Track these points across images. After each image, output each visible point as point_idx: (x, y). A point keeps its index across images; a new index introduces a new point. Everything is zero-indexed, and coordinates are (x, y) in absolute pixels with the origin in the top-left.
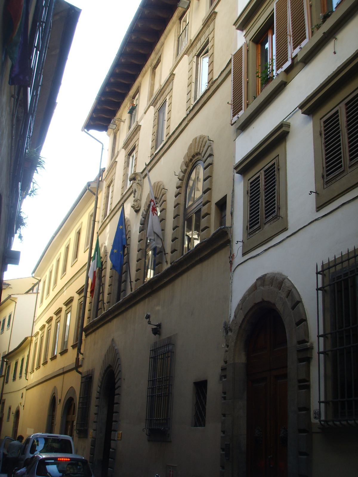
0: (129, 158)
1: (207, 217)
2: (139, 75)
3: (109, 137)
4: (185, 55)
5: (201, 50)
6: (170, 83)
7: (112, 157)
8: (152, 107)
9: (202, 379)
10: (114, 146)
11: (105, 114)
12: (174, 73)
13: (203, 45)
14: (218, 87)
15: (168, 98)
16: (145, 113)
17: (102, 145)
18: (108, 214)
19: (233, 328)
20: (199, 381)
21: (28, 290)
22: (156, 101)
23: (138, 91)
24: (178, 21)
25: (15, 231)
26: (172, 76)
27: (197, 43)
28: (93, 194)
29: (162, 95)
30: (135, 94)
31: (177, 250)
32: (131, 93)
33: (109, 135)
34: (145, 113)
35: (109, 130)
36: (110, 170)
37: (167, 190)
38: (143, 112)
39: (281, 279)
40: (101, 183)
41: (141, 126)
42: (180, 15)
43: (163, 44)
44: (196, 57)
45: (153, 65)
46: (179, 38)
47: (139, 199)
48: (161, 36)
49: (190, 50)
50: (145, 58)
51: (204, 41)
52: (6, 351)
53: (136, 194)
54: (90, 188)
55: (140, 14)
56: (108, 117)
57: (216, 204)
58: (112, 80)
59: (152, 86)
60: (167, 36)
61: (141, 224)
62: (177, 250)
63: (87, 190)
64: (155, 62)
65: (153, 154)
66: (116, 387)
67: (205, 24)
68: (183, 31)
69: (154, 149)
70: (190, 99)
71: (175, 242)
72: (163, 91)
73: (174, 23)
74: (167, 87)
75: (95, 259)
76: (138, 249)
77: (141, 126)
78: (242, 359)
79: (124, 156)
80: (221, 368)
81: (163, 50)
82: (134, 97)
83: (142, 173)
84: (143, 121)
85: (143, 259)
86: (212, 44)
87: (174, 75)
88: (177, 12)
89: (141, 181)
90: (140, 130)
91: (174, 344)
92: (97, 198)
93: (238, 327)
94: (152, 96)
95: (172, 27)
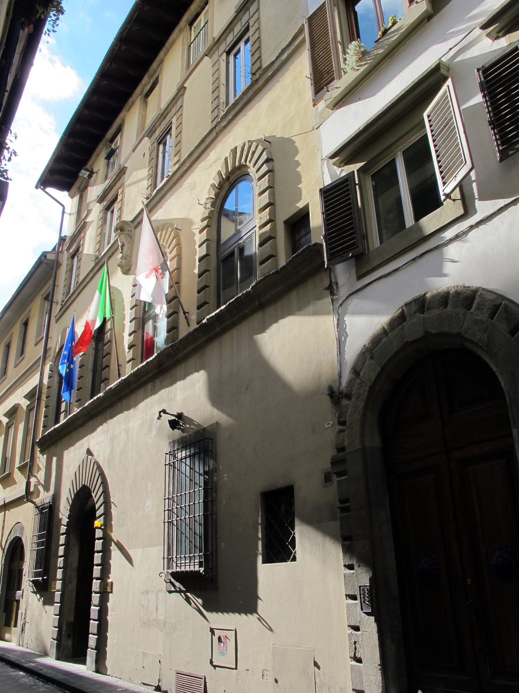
0: (106, 214)
4: (206, 57)
5: (242, 33)
6: (178, 100)
8: (146, 139)
9: (281, 484)
11: (67, 170)
12: (185, 85)
13: (237, 37)
15: (174, 120)
16: (134, 151)
17: (62, 208)
18: (71, 292)
19: (354, 392)
20: (273, 488)
21: (10, 297)
22: (154, 130)
23: (119, 130)
24: (188, 27)
25: (8, 88)
26: (182, 90)
27: (227, 36)
29: (163, 120)
30: (113, 135)
31: (208, 303)
32: (109, 134)
33: (72, 197)
34: (134, 151)
35: (74, 189)
37: (270, 142)
38: (131, 149)
39: (468, 292)
40: (60, 254)
41: (126, 168)
42: (190, 19)
43: (162, 61)
44: (225, 54)
45: (145, 92)
46: (190, 46)
47: (129, 255)
49: (214, 49)
50: (135, 82)
51: (241, 30)
53: (125, 248)
55: (135, 13)
56: (73, 169)
57: (286, 222)
58: (78, 127)
59: (143, 118)
60: (168, 50)
62: (208, 303)
64: (148, 87)
65: (64, 301)
66: (97, 516)
68: (195, 39)
69: (65, 296)
70: (179, 151)
71: (205, 291)
72: (165, 114)
73: (181, 31)
74: (173, 106)
77: (126, 168)
78: (374, 441)
79: (98, 211)
80: (330, 461)
81: (161, 69)
82: (112, 140)
83: (132, 221)
84: (129, 161)
85: (141, 331)
86: (257, 27)
87: (185, 88)
89: (131, 231)
91: (212, 439)
93: (367, 388)
94: (143, 129)
95: (178, 36)
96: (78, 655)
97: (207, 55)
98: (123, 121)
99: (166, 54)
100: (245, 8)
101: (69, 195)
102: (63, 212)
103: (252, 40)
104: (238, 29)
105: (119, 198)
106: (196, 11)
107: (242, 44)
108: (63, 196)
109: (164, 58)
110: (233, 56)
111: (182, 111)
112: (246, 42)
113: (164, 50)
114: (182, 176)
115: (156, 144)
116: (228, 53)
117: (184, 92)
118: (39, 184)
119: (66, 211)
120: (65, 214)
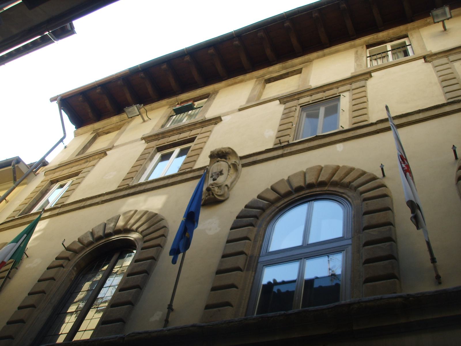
1: (150, 260)
2: (248, 73)
3: (75, 137)
7: (79, 153)
10: (88, 145)
12: (107, 152)
14: (173, 184)
16: (240, 110)
17: (62, 135)
26: (368, 76)
27: (318, 93)
28: (371, 55)
34: (240, 110)
36: (75, 162)
42: (371, 42)
48: (316, 51)
49: (97, 157)
51: (176, 140)
52: (174, 110)
54: (16, 165)
60: (324, 56)
61: (79, 239)
63: (10, 165)
67: (147, 149)
75: (17, 242)
76: (50, 265)
87: (371, 76)
88: (372, 36)
90: (216, 124)
92: (14, 188)
94: (83, 153)
96: (440, 283)
97: (279, 99)
98: (216, 92)
99: (318, 57)
100: (447, 54)
101: (75, 132)
102: (61, 140)
103: (66, 188)
104: (74, 169)
105: (80, 175)
106: (383, 39)
107: (177, 150)
108: (71, 127)
109: (313, 60)
110: (59, 185)
111: (92, 169)
112: (62, 186)
113: (320, 53)
114: (76, 209)
115: (152, 151)
116: (159, 149)
117: (103, 157)
118: (59, 98)
119: (64, 140)
120: (61, 143)
